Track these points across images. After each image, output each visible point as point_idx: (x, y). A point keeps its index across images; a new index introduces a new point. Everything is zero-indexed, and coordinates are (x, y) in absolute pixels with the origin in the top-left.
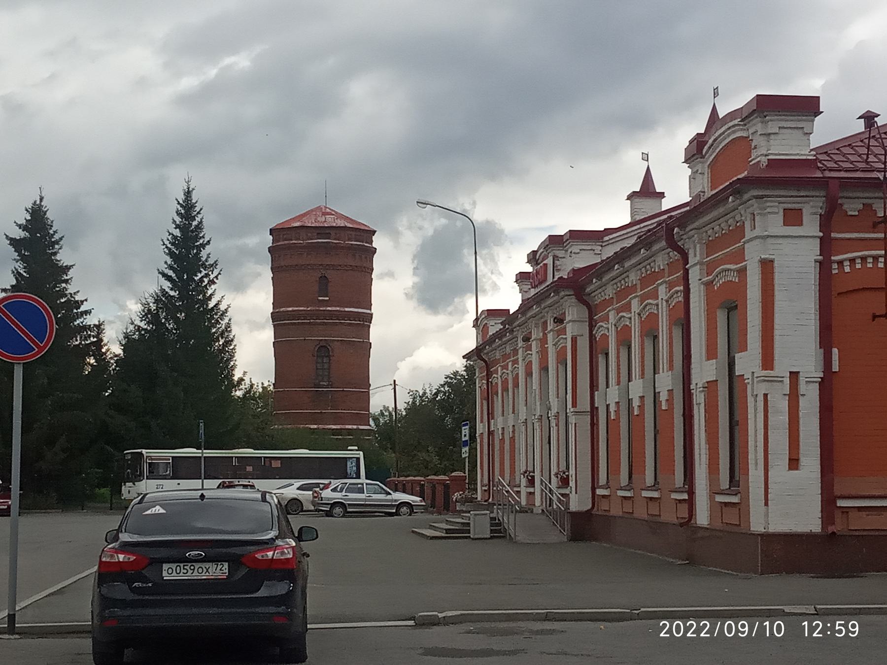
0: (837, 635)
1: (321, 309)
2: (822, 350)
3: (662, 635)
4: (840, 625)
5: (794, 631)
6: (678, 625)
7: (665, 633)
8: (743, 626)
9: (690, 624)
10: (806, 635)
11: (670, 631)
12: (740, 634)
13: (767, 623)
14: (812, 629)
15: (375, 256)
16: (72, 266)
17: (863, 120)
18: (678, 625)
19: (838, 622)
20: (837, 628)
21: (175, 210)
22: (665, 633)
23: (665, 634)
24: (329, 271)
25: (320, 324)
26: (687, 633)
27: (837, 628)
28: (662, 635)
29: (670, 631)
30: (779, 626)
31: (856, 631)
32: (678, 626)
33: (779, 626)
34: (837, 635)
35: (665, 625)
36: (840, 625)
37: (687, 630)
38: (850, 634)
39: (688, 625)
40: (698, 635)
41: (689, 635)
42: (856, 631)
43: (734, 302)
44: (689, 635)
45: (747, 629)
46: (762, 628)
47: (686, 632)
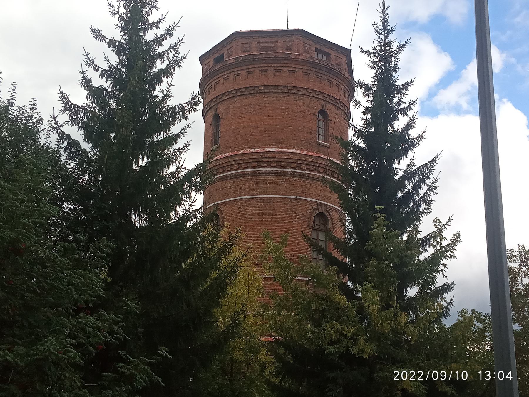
0: (485, 379)
1: (322, 156)
2: (111, 48)
3: (395, 379)
6: (404, 373)
7: (397, 378)
8: (443, 374)
10: (481, 379)
12: (441, 379)
13: (458, 372)
14: (484, 375)
15: (200, 76)
16: (433, 160)
22: (397, 378)
23: (420, 378)
25: (285, 174)
26: (410, 378)
28: (395, 379)
30: (465, 374)
31: (444, 377)
32: (404, 374)
33: (465, 374)
34: (485, 379)
38: (441, 379)
40: (417, 379)
42: (444, 377)
45: (445, 375)
46: (454, 374)
47: (409, 378)
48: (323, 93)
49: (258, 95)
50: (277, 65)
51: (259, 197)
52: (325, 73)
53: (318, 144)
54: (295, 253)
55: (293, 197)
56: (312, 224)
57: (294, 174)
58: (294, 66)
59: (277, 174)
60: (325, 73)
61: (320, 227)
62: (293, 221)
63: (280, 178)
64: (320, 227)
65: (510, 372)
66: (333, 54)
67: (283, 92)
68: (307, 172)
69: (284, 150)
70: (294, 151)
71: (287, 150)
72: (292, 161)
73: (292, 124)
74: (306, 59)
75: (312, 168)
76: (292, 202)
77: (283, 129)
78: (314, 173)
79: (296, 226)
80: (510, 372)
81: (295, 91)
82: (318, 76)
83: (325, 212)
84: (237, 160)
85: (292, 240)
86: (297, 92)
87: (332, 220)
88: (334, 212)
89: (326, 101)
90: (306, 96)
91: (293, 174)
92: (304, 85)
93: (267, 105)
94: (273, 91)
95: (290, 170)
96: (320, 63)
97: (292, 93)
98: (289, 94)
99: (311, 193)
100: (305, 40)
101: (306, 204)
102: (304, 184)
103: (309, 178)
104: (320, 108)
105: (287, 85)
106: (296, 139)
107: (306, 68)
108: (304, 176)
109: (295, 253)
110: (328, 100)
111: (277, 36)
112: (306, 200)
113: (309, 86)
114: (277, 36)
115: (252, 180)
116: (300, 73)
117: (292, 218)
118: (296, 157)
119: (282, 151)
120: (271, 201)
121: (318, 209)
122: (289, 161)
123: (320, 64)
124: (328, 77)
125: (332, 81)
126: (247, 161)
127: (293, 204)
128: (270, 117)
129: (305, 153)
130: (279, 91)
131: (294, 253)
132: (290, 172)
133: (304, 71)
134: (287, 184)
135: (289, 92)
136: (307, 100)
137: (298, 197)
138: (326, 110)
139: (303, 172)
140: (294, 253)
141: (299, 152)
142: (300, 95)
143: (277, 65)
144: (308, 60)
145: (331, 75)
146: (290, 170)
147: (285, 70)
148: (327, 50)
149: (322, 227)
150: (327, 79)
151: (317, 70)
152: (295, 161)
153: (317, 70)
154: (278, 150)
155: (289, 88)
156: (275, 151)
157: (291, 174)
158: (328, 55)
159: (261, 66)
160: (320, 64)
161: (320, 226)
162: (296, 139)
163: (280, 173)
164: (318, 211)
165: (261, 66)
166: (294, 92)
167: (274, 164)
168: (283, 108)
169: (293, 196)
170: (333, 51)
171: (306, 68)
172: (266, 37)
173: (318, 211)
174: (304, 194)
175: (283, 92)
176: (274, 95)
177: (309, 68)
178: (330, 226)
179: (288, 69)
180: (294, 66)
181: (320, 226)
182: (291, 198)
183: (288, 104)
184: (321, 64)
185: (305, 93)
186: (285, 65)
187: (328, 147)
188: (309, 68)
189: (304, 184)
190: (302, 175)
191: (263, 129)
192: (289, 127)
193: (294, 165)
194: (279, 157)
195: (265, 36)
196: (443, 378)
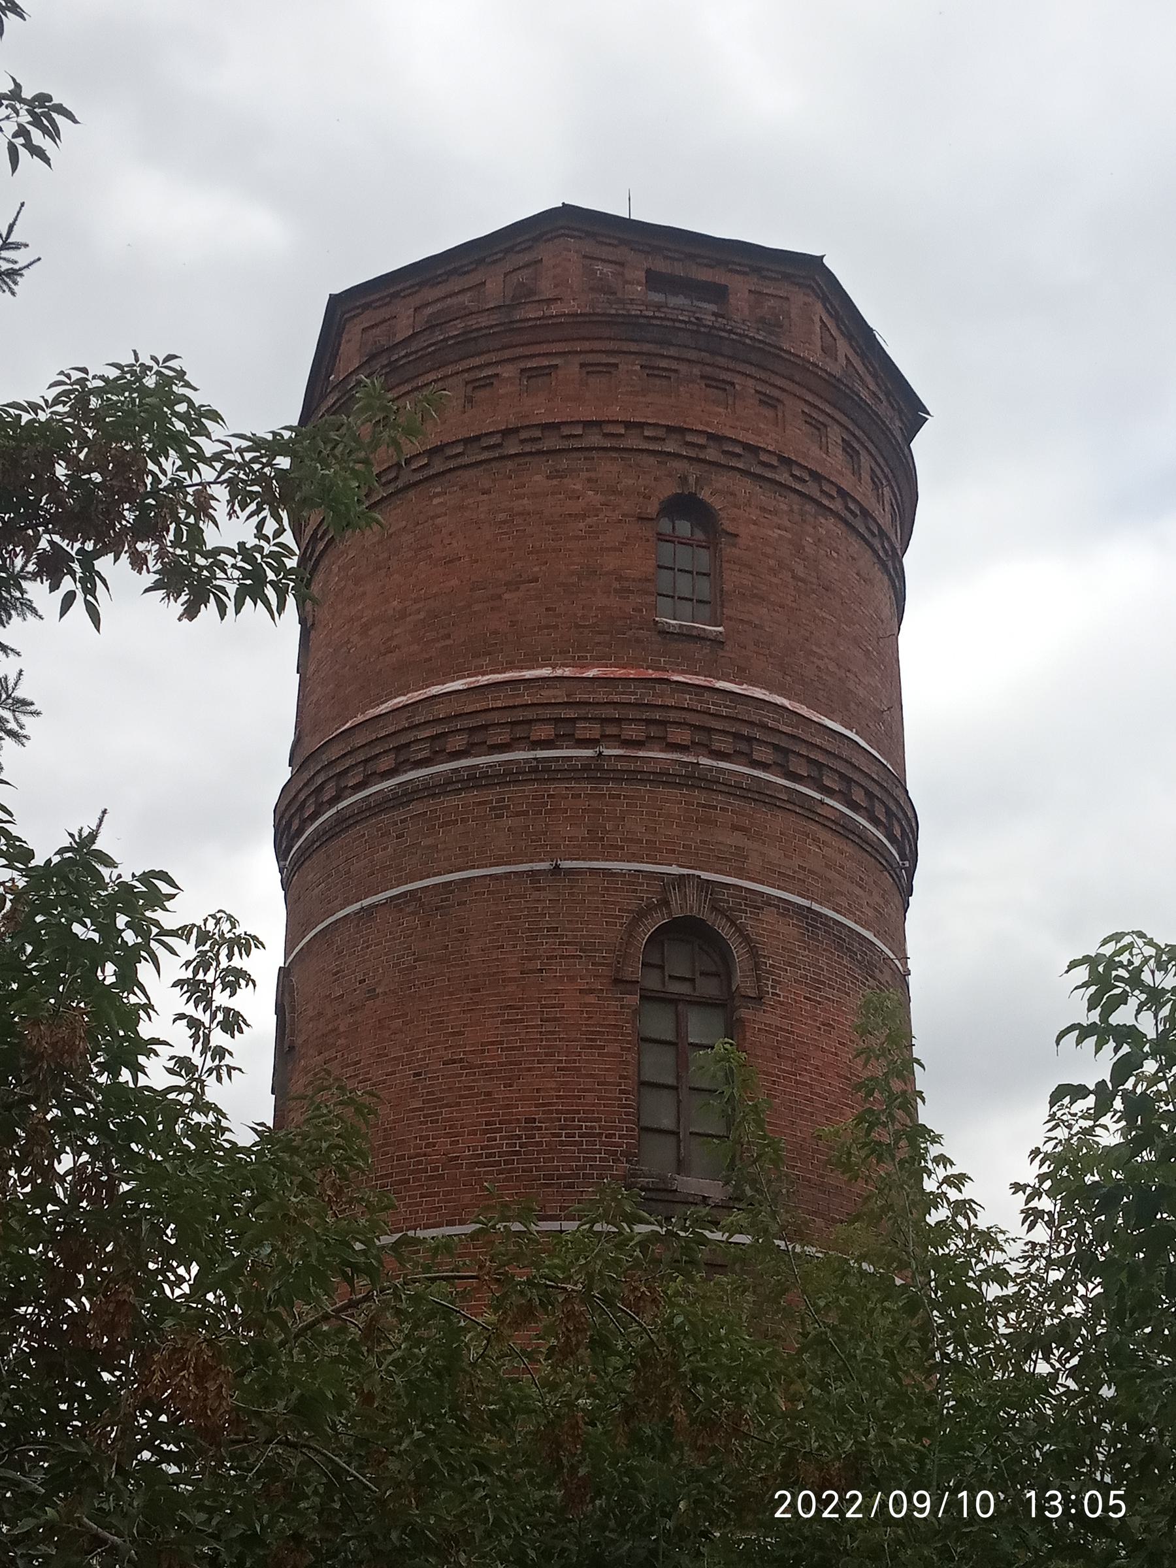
3: (778, 1515)
4: (1116, 1497)
5: (76, 1409)
8: (922, 1499)
9: (827, 1496)
11: (792, 1507)
12: (915, 1514)
17: (12, 86)
18: (807, 1497)
19: (1113, 1493)
20: (1112, 1502)
21: (26, 727)
23: (783, 1513)
24: (722, 480)
25: (662, 778)
27: (1112, 1502)
28: (778, 1515)
29: (792, 1507)
30: (985, 1499)
35: (783, 1497)
36: (1116, 1497)
37: (824, 1503)
38: (915, 1514)
39: (824, 1497)
41: (826, 1515)
43: (929, 414)
44: (826, 1515)
45: (928, 1504)
46: (955, 1504)
48: (682, 431)
49: (411, 494)
50: (477, 361)
51: (404, 894)
52: (692, 355)
53: (664, 633)
54: (551, 1112)
55: (545, 866)
56: (634, 970)
57: (547, 770)
58: (544, 348)
59: (475, 779)
60: (692, 355)
61: (694, 989)
62: (541, 971)
63: (491, 795)
64: (694, 989)
65: (145, 889)
66: (740, 288)
67: (502, 458)
68: (607, 752)
69: (503, 675)
70: (545, 672)
71: (512, 674)
72: (530, 714)
73: (536, 569)
74: (587, 310)
75: (632, 731)
76: (538, 889)
77: (500, 597)
78: (641, 754)
79: (557, 992)
80: (145, 889)
81: (551, 442)
82: (658, 368)
83: (706, 915)
84: (331, 763)
85: (535, 1054)
86: (560, 445)
87: (753, 952)
88: (769, 916)
89: (704, 461)
90: (601, 454)
91: (541, 771)
92: (587, 413)
93: (438, 521)
94: (465, 460)
95: (530, 755)
96: (655, 317)
97: (540, 453)
98: (528, 459)
99: (631, 840)
100: (589, 247)
101: (607, 889)
102: (596, 804)
103: (620, 776)
104: (669, 489)
105: (513, 422)
106: (556, 627)
107: (597, 345)
108: (592, 771)
109: (551, 1112)
110: (712, 454)
111: (482, 261)
112: (607, 872)
113: (615, 412)
114: (482, 261)
115: (381, 828)
116: (572, 369)
117: (539, 958)
118: (547, 695)
119: (490, 681)
120: (447, 899)
121: (665, 903)
122: (520, 715)
123: (655, 322)
124: (709, 369)
125: (733, 384)
126: (361, 757)
127: (542, 895)
128: (450, 562)
129: (591, 673)
130: (485, 455)
131: (544, 1112)
132: (526, 761)
133: (590, 358)
134: (518, 814)
135: (528, 449)
136: (608, 469)
137: (566, 864)
138: (704, 495)
139: (589, 753)
140: (544, 1112)
141: (567, 672)
142: (575, 455)
143: (477, 361)
144: (598, 310)
145: (721, 361)
146: (530, 755)
147: (508, 371)
148: (704, 275)
149: (709, 988)
150: (702, 377)
151: (646, 347)
152: (548, 713)
153: (646, 347)
154: (478, 681)
155: (524, 435)
156: (461, 688)
157: (534, 770)
158: (718, 293)
159: (420, 382)
160: (655, 322)
161: (692, 980)
162: (556, 627)
163: (485, 776)
164: (670, 914)
165: (420, 382)
166: (545, 446)
167: (457, 742)
168: (501, 516)
169: (543, 860)
170: (737, 276)
171: (597, 345)
172: (445, 277)
173: (670, 914)
174: (599, 844)
175: (502, 458)
176: (466, 476)
177: (612, 345)
178: (741, 979)
179: (522, 365)
180: (544, 348)
181: (692, 980)
182: (533, 873)
183: (519, 497)
184: (661, 318)
185: (595, 439)
186: (507, 354)
187: (717, 642)
188: (612, 345)
189: (596, 804)
190: (586, 768)
191: (422, 615)
192: (524, 582)
193: (543, 732)
194: (478, 707)
195: (440, 275)
196: (922, 1511)
